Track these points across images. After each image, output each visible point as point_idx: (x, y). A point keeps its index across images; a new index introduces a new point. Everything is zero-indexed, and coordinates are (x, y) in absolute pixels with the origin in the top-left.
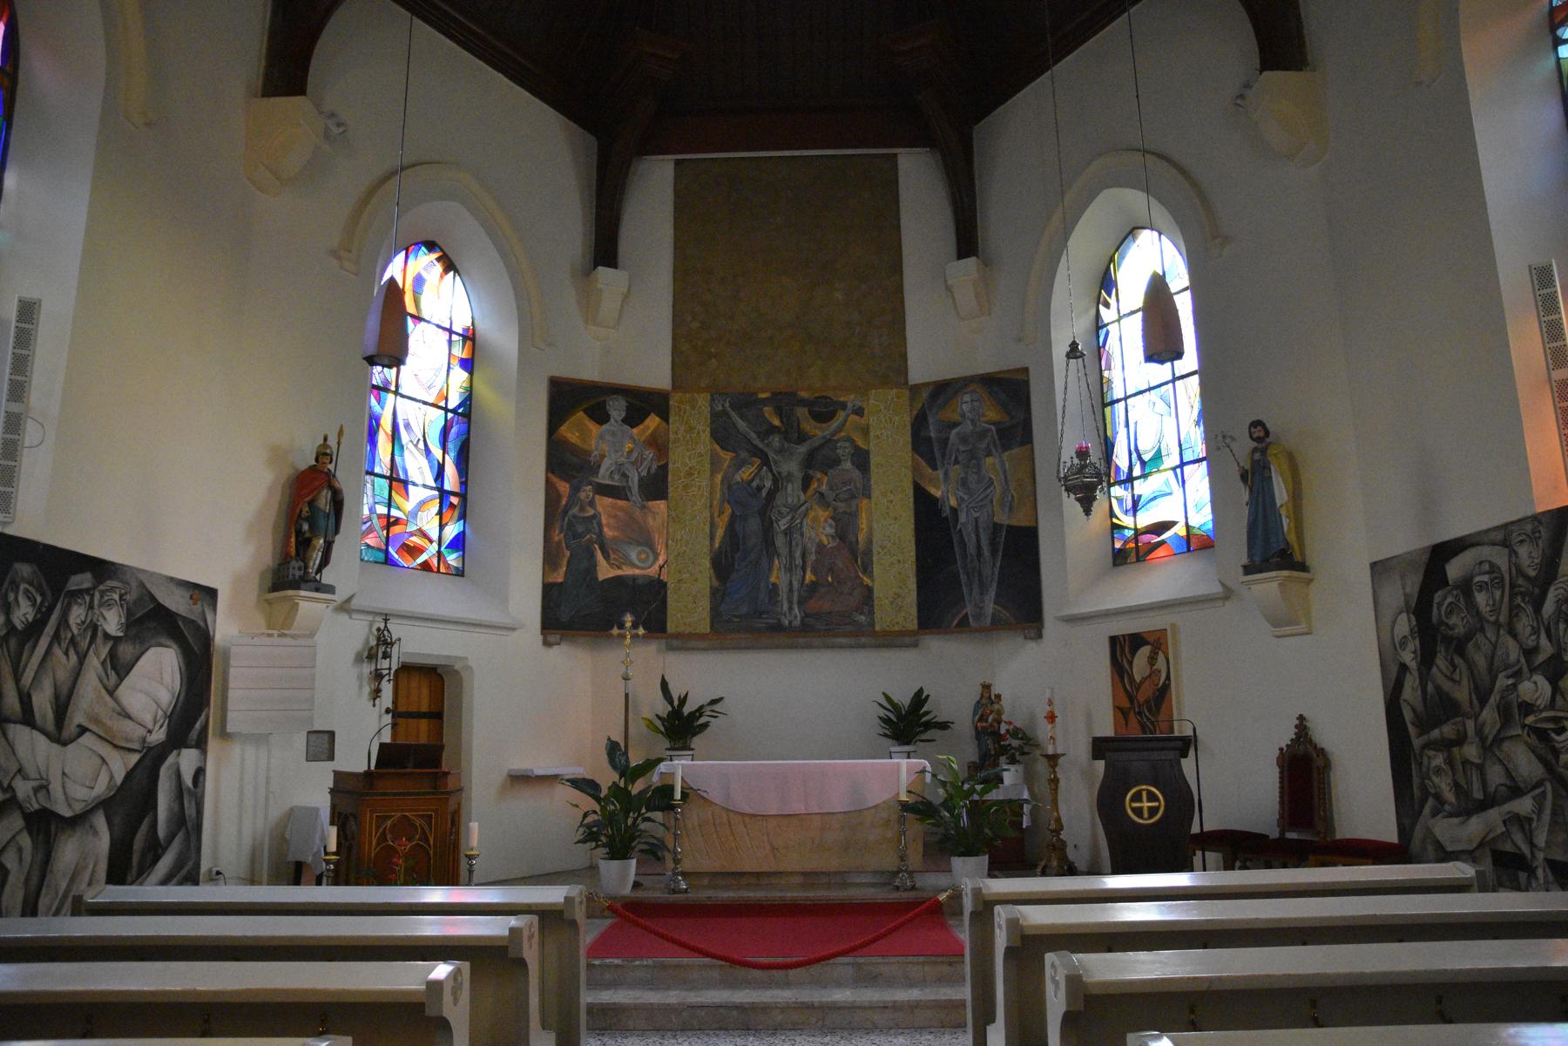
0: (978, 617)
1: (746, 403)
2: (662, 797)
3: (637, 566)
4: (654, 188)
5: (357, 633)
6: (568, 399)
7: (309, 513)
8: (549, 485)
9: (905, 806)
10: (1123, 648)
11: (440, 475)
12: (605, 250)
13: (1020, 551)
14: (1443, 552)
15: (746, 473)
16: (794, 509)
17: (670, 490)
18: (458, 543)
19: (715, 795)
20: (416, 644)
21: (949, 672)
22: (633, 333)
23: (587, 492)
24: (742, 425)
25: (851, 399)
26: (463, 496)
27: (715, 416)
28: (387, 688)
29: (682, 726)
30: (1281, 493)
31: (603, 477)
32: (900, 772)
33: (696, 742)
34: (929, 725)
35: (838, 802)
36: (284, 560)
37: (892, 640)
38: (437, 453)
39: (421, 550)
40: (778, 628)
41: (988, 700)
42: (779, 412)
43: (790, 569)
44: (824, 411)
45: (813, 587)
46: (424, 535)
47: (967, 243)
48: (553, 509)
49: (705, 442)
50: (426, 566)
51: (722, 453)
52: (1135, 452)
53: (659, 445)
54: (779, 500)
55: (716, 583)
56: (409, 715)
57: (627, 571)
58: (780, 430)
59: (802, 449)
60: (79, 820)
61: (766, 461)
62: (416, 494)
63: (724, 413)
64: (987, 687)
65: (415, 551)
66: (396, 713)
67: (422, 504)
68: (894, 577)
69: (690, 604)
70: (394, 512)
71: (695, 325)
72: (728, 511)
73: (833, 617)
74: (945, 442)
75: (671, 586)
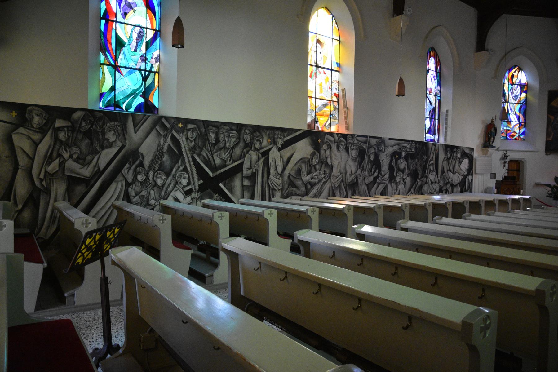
7: (490, 133)
18: (524, 133)
20: (513, 156)
46: (515, 132)
50: (516, 139)
67: (514, 126)
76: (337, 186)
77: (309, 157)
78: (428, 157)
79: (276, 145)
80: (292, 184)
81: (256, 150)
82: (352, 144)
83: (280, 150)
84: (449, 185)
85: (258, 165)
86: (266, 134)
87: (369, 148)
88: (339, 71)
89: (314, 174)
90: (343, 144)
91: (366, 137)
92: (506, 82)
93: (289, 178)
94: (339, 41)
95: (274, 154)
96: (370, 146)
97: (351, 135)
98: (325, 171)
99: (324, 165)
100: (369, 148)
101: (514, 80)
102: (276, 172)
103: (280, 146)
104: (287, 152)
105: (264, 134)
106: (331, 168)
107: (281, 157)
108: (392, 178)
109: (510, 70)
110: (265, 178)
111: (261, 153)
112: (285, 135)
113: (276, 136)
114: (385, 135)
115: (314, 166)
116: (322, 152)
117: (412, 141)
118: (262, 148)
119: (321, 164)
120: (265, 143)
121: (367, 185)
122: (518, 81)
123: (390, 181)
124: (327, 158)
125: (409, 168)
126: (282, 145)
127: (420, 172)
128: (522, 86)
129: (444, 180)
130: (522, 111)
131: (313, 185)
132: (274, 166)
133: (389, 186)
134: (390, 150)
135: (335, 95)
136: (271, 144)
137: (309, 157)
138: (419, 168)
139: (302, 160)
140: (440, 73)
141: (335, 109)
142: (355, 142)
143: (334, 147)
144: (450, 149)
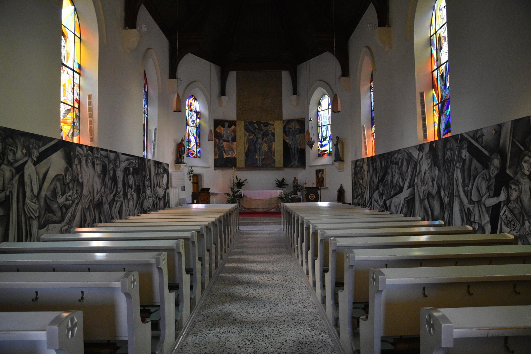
0: (294, 165)
1: (251, 123)
2: (240, 196)
3: (231, 155)
4: (232, 77)
6: (218, 123)
7: (181, 150)
9: (278, 198)
10: (318, 172)
11: (196, 140)
12: (223, 92)
13: (302, 154)
14: (357, 161)
15: (251, 137)
16: (260, 144)
18: (199, 152)
19: (248, 196)
20: (196, 171)
21: (288, 175)
23: (221, 141)
24: (250, 127)
25: (271, 122)
26: (200, 143)
27: (245, 126)
28: (192, 178)
29: (240, 184)
30: (340, 149)
32: (278, 192)
33: (242, 187)
34: (285, 185)
35: (268, 197)
37: (279, 169)
40: (257, 167)
41: (295, 180)
42: (257, 125)
43: (260, 155)
44: (266, 125)
45: (264, 159)
46: (194, 151)
47: (295, 92)
50: (194, 157)
52: (322, 137)
53: (234, 131)
54: (257, 142)
57: (229, 156)
58: (258, 130)
59: (262, 132)
61: (255, 135)
62: (193, 144)
64: (295, 178)
65: (193, 154)
67: (194, 146)
68: (279, 157)
69: (241, 161)
73: (267, 164)
74: (289, 131)
75: (237, 159)
76: (87, 207)
77: (63, 173)
78: (145, 172)
79: (31, 157)
80: (49, 209)
81: (10, 164)
82: (97, 158)
83: (35, 164)
84: (158, 199)
85: (13, 186)
86: (20, 142)
87: (109, 163)
88: (79, 74)
89: (68, 195)
90: (90, 158)
91: (106, 150)
92: (187, 108)
93: (45, 200)
94: (80, 39)
95: (30, 169)
96: (110, 161)
97: (96, 148)
98: (77, 191)
99: (76, 183)
100: (109, 163)
101: (192, 107)
102: (31, 194)
103: (35, 159)
104: (42, 167)
105: (17, 141)
106: (81, 185)
107: (37, 173)
108: (125, 195)
109: (189, 99)
110: (21, 203)
111: (15, 169)
112: (41, 145)
113: (31, 146)
114: (120, 150)
115: (68, 184)
116: (74, 167)
117: (136, 157)
118: (16, 161)
119: (73, 182)
120: (19, 154)
121: (109, 204)
122: (194, 109)
123: (124, 199)
124: (78, 175)
125: (135, 185)
126: (37, 158)
127: (141, 187)
128: (197, 113)
129: (155, 195)
130: (198, 133)
131: (67, 207)
132: (30, 186)
133: (124, 204)
134: (123, 165)
135: (77, 100)
136: (26, 156)
137: (63, 173)
138: (141, 184)
139: (57, 177)
140: (147, 92)
141: (77, 116)
142: (99, 156)
143: (84, 162)
144: (158, 164)
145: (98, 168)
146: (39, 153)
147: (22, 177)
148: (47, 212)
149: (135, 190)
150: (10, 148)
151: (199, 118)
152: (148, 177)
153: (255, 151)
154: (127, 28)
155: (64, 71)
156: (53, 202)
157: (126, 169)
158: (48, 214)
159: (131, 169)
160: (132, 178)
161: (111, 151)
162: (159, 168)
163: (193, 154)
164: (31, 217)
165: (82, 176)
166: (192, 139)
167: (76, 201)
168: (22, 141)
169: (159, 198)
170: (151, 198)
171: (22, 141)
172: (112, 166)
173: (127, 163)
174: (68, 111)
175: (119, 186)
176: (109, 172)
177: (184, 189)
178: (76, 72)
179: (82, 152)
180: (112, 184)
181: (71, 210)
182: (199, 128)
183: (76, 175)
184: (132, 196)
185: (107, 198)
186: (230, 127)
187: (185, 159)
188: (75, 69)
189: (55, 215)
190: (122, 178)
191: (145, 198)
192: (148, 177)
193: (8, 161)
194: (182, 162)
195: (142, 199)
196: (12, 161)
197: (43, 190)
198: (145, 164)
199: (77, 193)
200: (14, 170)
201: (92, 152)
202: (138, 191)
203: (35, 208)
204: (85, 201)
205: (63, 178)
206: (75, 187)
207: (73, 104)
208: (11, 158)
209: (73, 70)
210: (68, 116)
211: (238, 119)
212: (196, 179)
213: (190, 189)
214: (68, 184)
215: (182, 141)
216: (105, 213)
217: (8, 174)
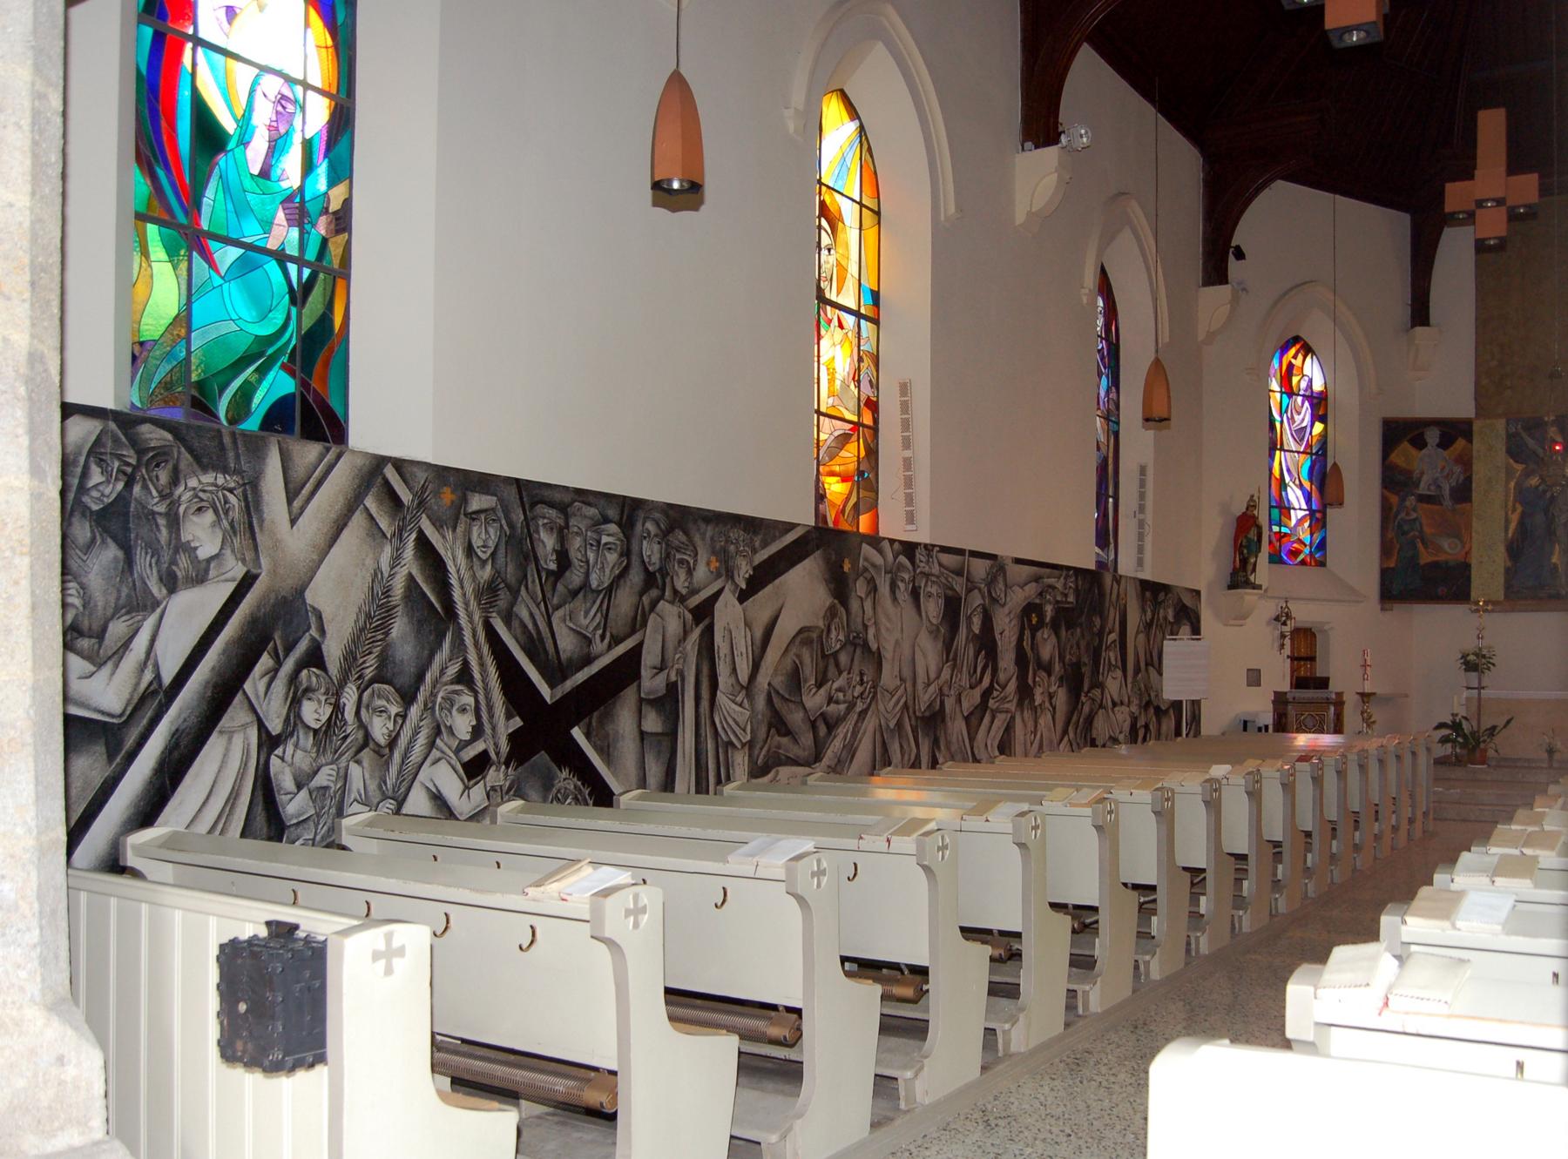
3: (1449, 549)
5: (1270, 608)
6: (1399, 433)
7: (1247, 537)
8: (1384, 500)
11: (1308, 500)
12: (1420, 314)
17: (1474, 494)
20: (1304, 614)
22: (1442, 380)
27: (1511, 437)
28: (1287, 641)
31: (1423, 489)
36: (1234, 573)
38: (1307, 485)
39: (1298, 552)
46: (1300, 541)
48: (1386, 511)
49: (1501, 456)
50: (1303, 563)
51: (1516, 466)
53: (1466, 462)
55: (1509, 564)
56: (1299, 659)
57: (1442, 558)
60: (1166, 711)
62: (1295, 516)
63: (1516, 435)
65: (1297, 553)
66: (1293, 658)
67: (1300, 521)
70: (1284, 530)
71: (1494, 363)
72: (1519, 509)
76: (892, 725)
77: (821, 624)
78: (1104, 619)
79: (732, 578)
80: (778, 724)
82: (927, 575)
83: (743, 597)
87: (969, 591)
88: (875, 321)
89: (835, 686)
90: (906, 576)
91: (960, 552)
93: (769, 700)
95: (728, 612)
97: (926, 546)
98: (862, 675)
99: (858, 651)
100: (969, 591)
101: (1295, 380)
102: (733, 680)
105: (697, 539)
106: (877, 659)
107: (746, 624)
108: (1025, 692)
110: (705, 704)
111: (691, 611)
112: (757, 544)
113: (732, 548)
115: (835, 655)
116: (854, 605)
118: (694, 592)
119: (850, 648)
120: (701, 572)
121: (967, 719)
122: (1303, 385)
123: (1020, 704)
124: (866, 627)
125: (1062, 658)
126: (750, 581)
127: (1086, 670)
128: (1319, 403)
131: (832, 726)
134: (1019, 598)
136: (719, 576)
137: (821, 624)
138: (1085, 659)
142: (936, 569)
144: (1153, 591)
145: (933, 608)
146: (754, 569)
147: (709, 631)
148: (773, 731)
149: (1061, 679)
150: (678, 556)
151: (1323, 419)
152: (1113, 636)
153: (1550, 533)
154: (1029, 145)
155: (829, 322)
156: (792, 706)
157: (1030, 609)
158: (777, 738)
159: (1049, 609)
160: (1053, 639)
161: (974, 554)
162: (1157, 604)
163: (1297, 553)
164: (731, 743)
165: (878, 630)
166: (1295, 496)
167: (860, 706)
168: (709, 534)
169: (1157, 709)
170: (1124, 708)
171: (709, 534)
172: (979, 601)
173: (1031, 589)
174: (844, 440)
175: (1002, 664)
176: (969, 618)
177: (1254, 678)
178: (867, 318)
179: (878, 560)
180: (976, 658)
181: (843, 731)
182: (1320, 455)
183: (860, 627)
184: (1051, 696)
185: (959, 701)
186: (1445, 443)
187: (1263, 570)
188: (863, 311)
189: (796, 741)
190: (1014, 639)
191: (1101, 706)
192: (1113, 636)
193: (675, 592)
194: (1248, 584)
195: (1086, 709)
196: (684, 592)
197: (762, 671)
198: (1102, 595)
199: (862, 682)
200: (689, 616)
201: (912, 559)
202: (1074, 682)
203: (741, 720)
204: (888, 709)
205: (820, 637)
206: (856, 662)
207: (859, 415)
208: (681, 583)
209: (857, 314)
210: (843, 453)
211: (1481, 410)
212: (1304, 646)
213: (1278, 676)
214: (835, 655)
215: (1252, 505)
216: (954, 747)
217: (674, 627)
